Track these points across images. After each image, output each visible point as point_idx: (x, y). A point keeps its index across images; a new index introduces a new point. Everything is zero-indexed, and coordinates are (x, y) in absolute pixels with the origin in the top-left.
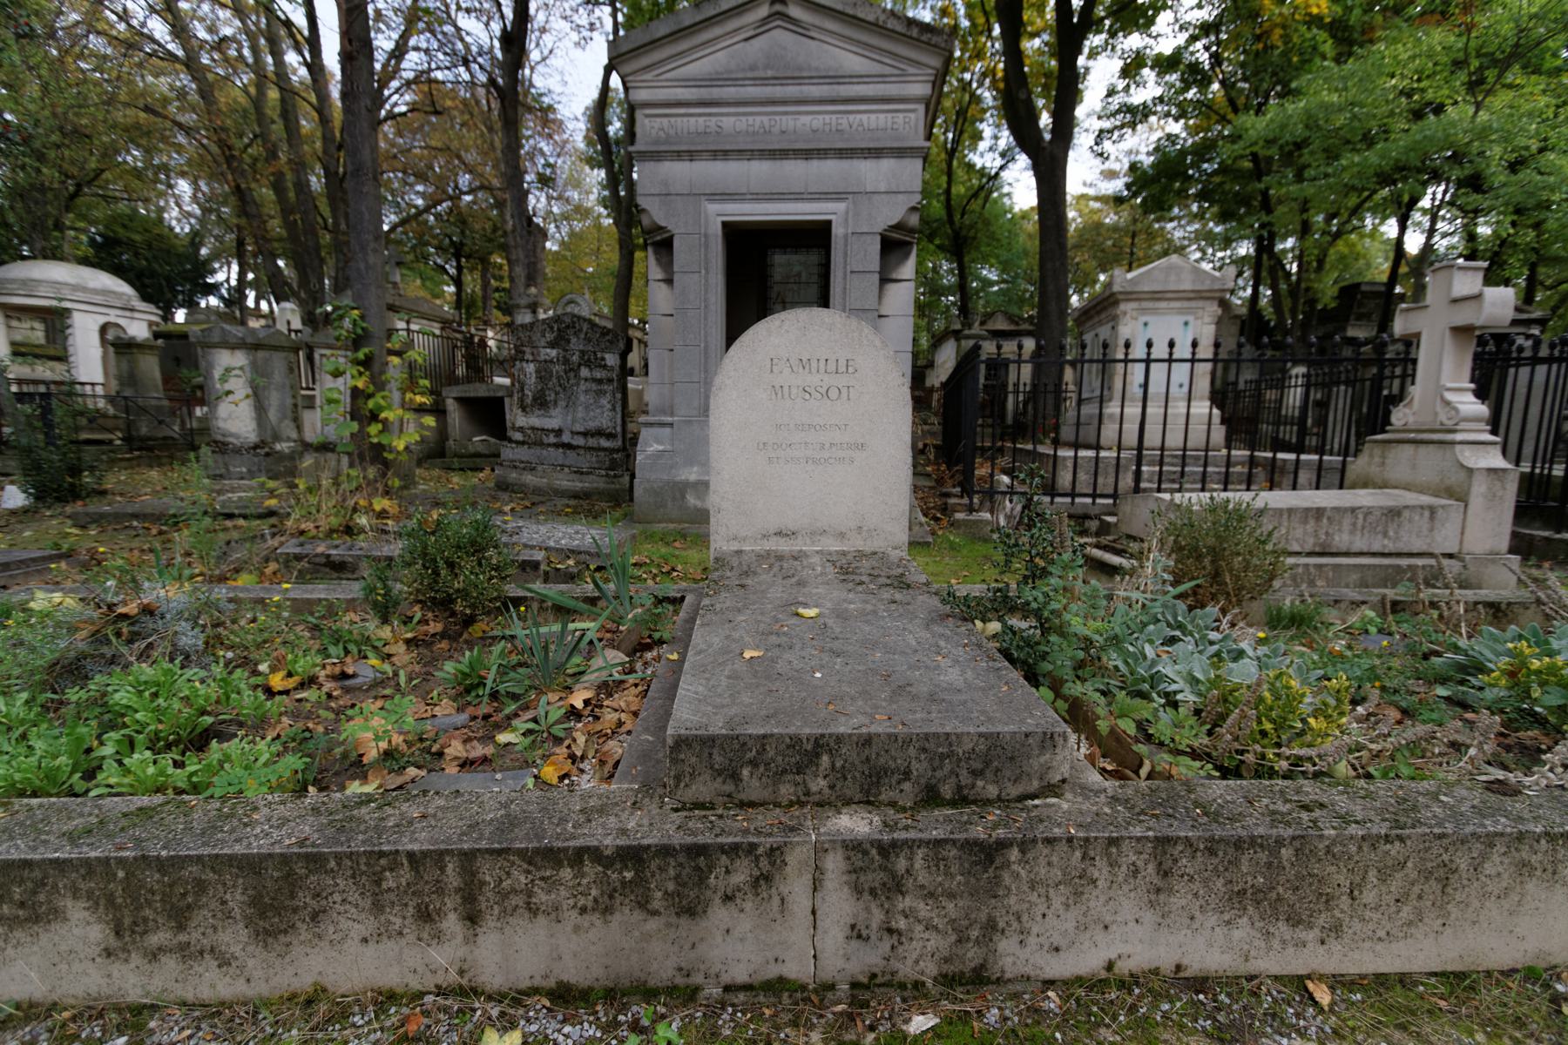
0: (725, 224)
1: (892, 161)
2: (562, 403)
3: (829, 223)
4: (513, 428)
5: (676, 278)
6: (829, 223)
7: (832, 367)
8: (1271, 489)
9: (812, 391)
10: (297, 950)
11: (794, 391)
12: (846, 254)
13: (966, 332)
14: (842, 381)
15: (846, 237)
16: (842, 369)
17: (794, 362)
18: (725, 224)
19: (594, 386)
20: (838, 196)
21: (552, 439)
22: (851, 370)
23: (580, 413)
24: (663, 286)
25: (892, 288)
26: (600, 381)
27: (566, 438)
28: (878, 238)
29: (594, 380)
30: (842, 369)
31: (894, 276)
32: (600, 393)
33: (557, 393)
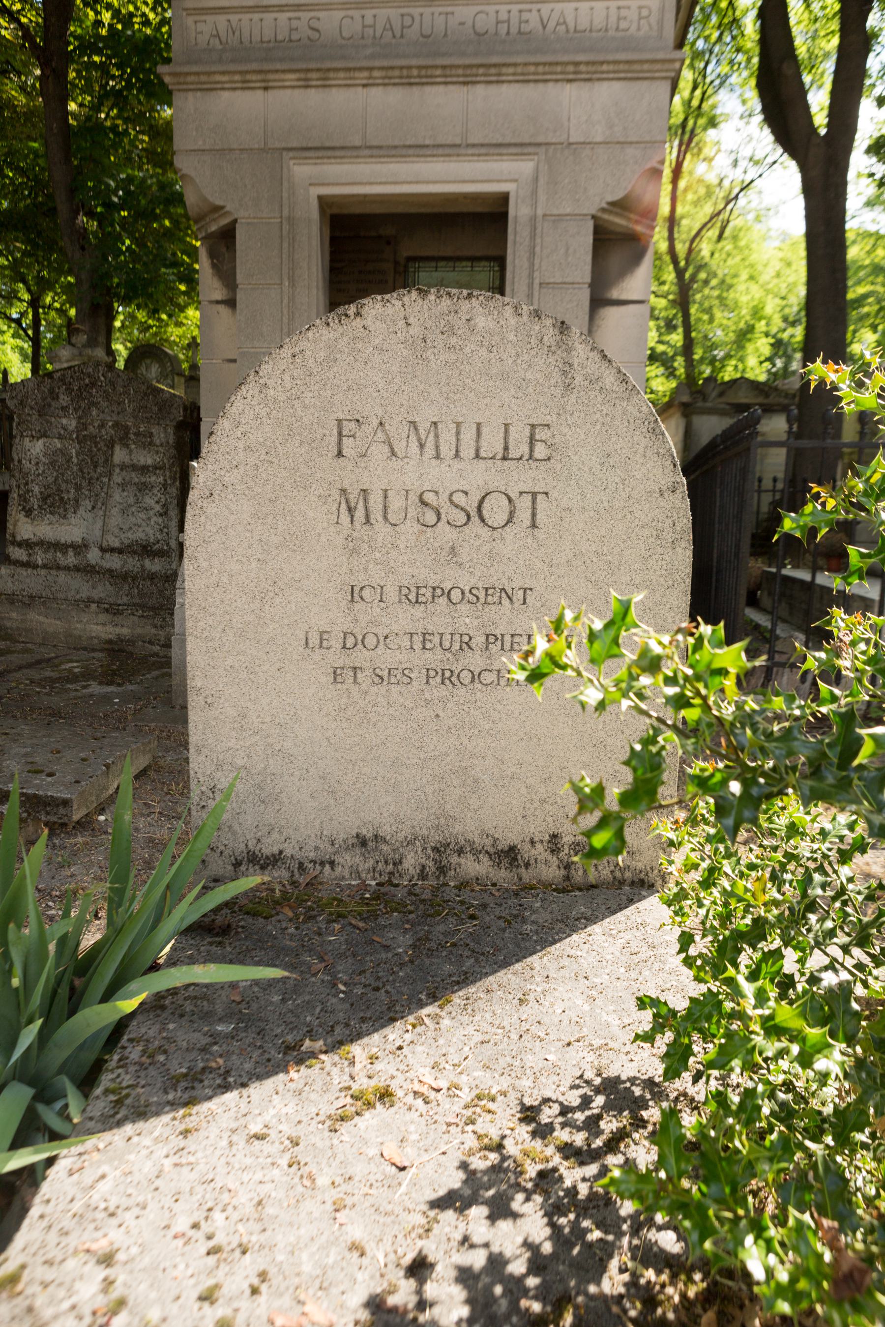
0: (320, 198)
1: (617, 86)
2: (87, 504)
3: (504, 199)
4: (14, 543)
5: (240, 296)
6: (504, 199)
7: (492, 443)
8: (198, 380)
9: (442, 502)
10: (721, 267)
11: (396, 503)
12: (532, 253)
13: (700, 404)
14: (520, 478)
15: (533, 219)
16: (520, 448)
17: (397, 430)
18: (320, 198)
19: (135, 477)
20: (519, 148)
21: (71, 559)
22: (540, 451)
23: (115, 519)
24: (223, 309)
25: (611, 314)
26: (144, 469)
27: (93, 556)
28: (590, 224)
29: (134, 467)
30: (520, 448)
31: (615, 294)
32: (143, 488)
33: (78, 488)
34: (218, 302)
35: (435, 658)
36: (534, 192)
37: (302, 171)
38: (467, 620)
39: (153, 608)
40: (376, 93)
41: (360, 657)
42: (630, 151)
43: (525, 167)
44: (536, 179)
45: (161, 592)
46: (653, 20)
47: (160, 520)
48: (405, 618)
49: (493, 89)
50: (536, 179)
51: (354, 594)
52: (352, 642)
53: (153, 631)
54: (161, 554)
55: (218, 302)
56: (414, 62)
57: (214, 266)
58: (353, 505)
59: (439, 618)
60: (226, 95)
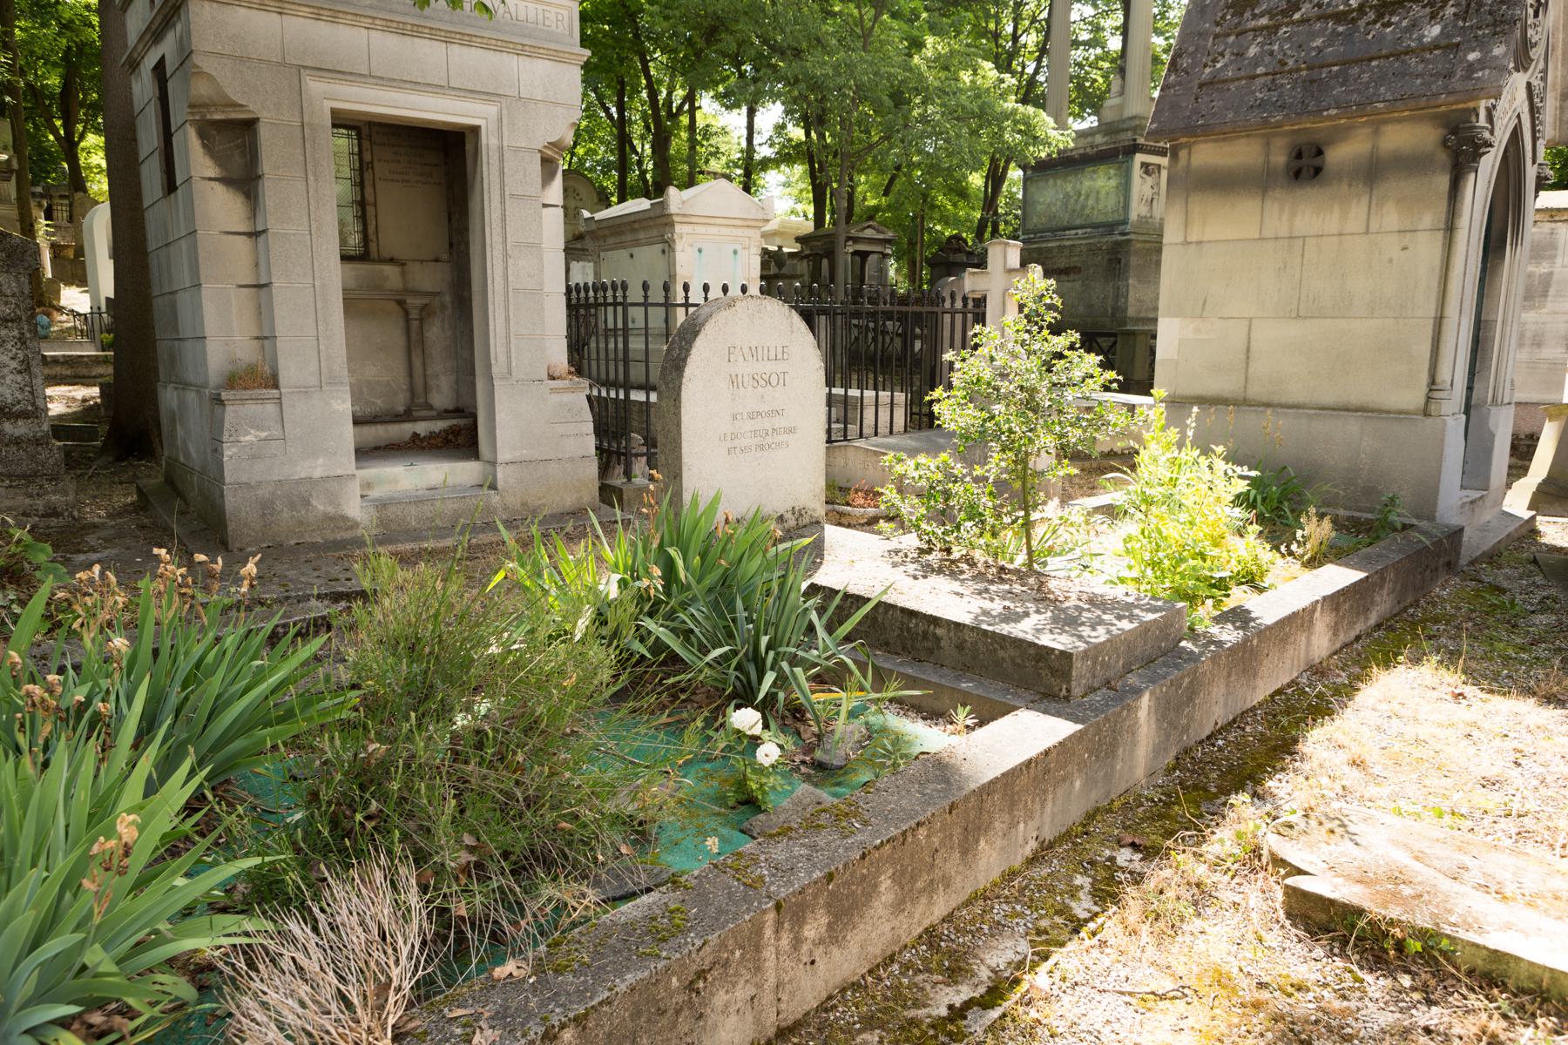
6: (475, 130)
7: (772, 356)
34: (210, 179)
35: (758, 440)
36: (500, 128)
37: (315, 86)
38: (767, 424)
39: (24, 476)
40: (376, 35)
41: (736, 443)
42: (560, 109)
43: (491, 110)
44: (500, 120)
45: (33, 457)
46: (566, 23)
47: (19, 378)
48: (748, 425)
49: (465, 50)
50: (500, 120)
51: (734, 417)
52: (734, 436)
53: (28, 501)
54: (24, 415)
55: (210, 179)
56: (410, 20)
57: (204, 146)
58: (734, 381)
59: (759, 424)
60: (243, 10)
